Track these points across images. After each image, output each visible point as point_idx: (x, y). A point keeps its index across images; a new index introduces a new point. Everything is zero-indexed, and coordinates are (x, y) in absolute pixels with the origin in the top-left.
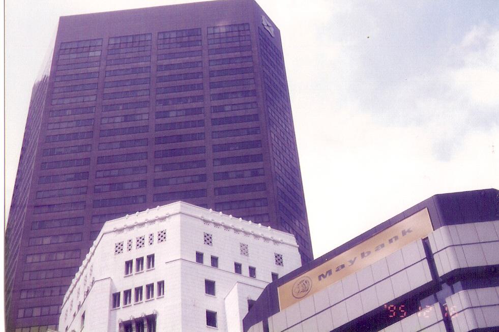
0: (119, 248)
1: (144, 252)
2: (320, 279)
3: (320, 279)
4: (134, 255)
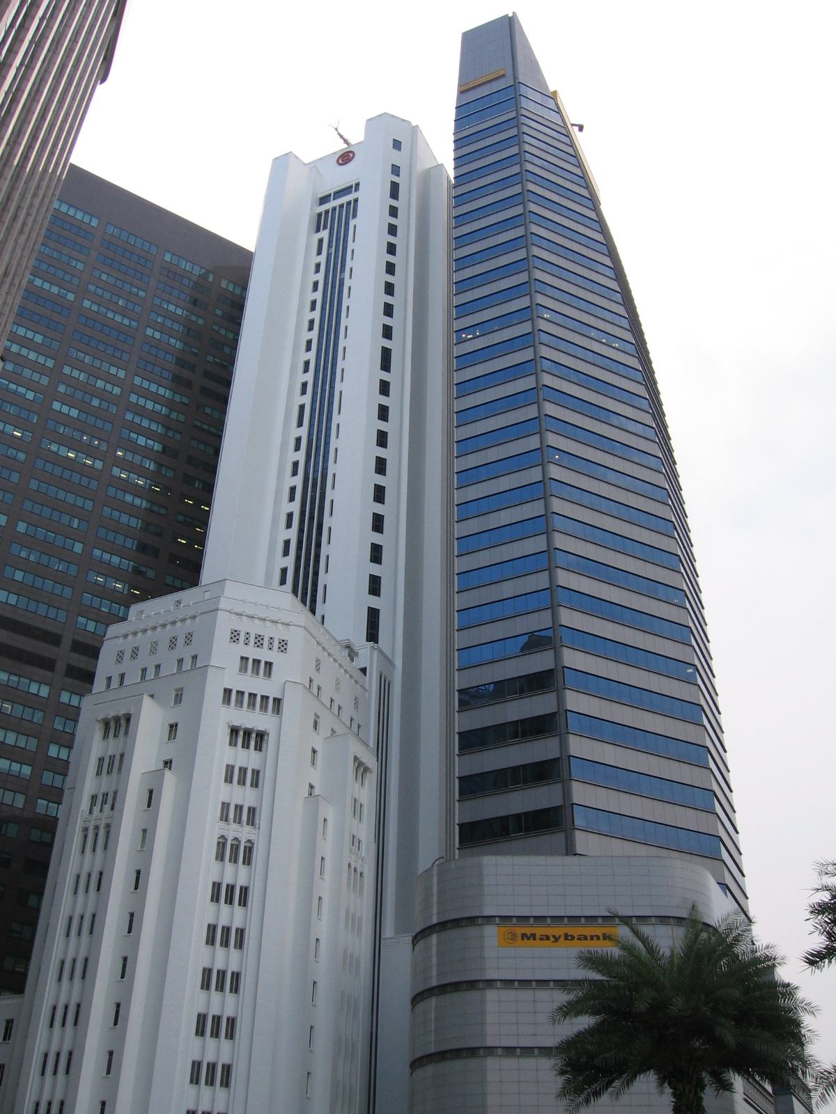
0: (235, 637)
1: (264, 655)
2: (523, 939)
3: (523, 939)
4: (252, 653)
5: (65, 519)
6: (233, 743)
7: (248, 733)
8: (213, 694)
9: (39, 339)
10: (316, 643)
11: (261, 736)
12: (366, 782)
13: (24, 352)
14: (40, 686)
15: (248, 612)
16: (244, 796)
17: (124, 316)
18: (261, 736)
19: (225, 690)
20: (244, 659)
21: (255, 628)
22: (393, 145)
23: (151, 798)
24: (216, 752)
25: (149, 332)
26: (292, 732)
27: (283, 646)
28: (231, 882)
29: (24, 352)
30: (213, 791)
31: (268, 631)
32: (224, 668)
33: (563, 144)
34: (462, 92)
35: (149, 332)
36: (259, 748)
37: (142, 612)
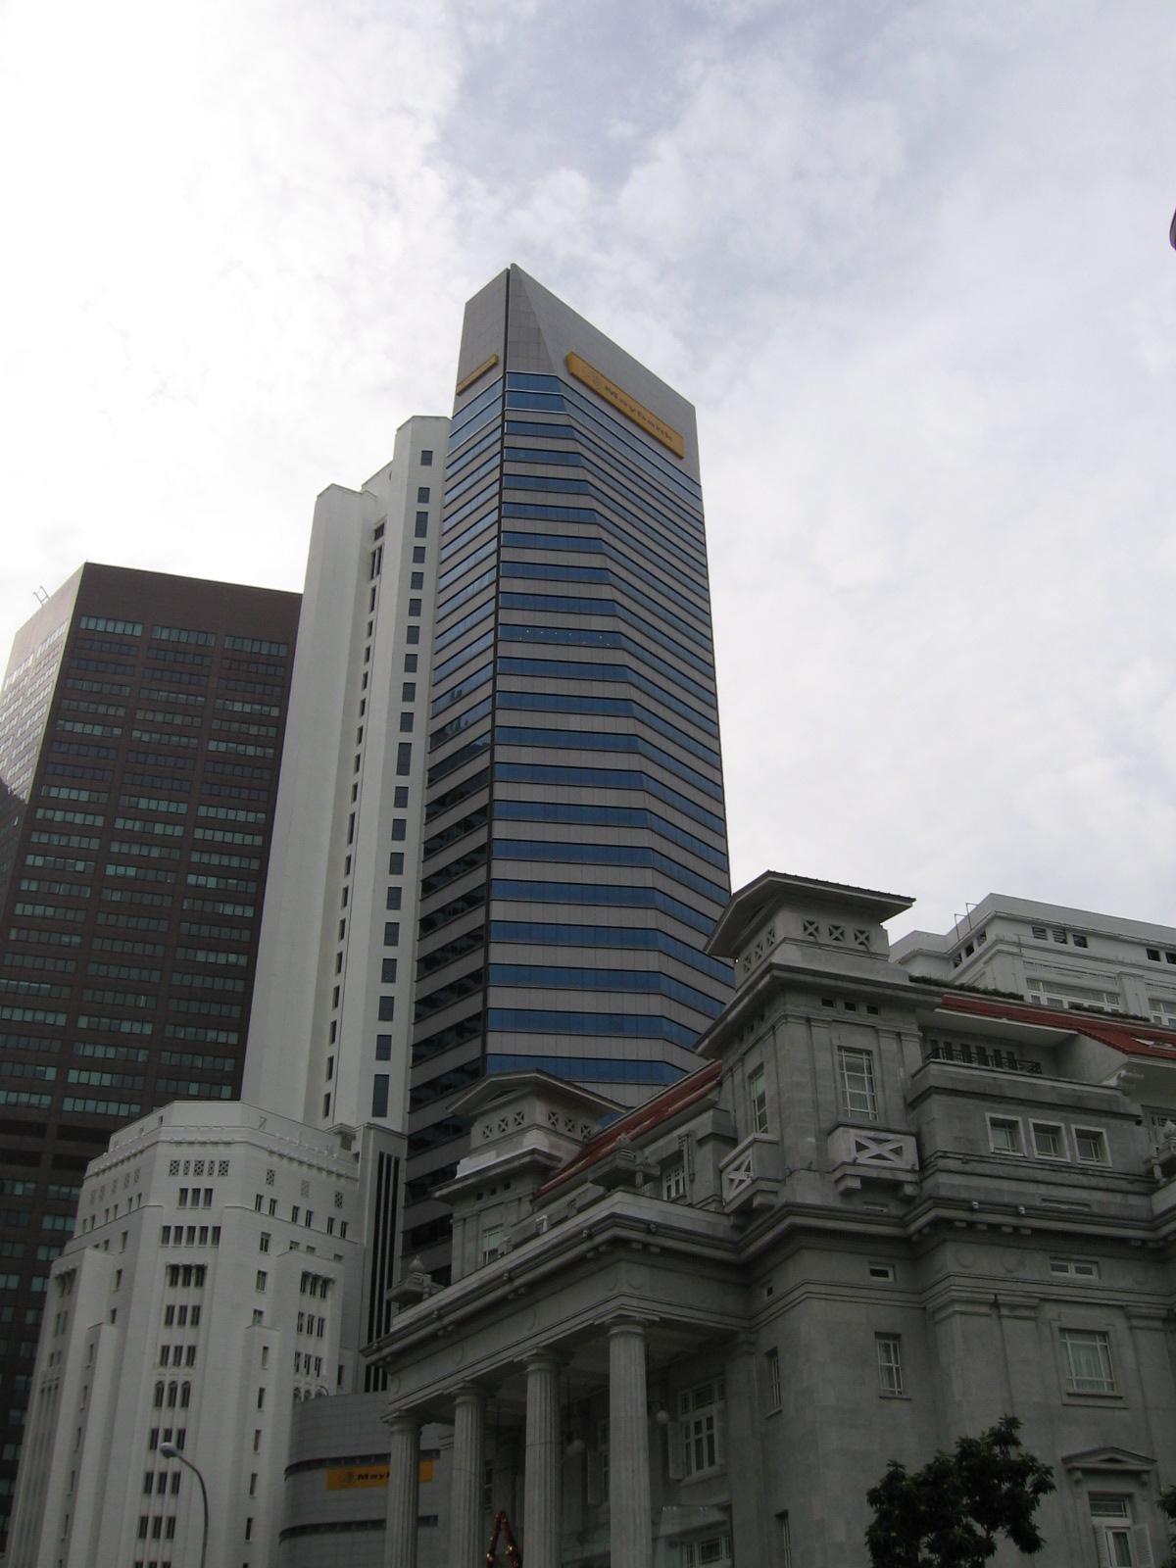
1: (203, 1182)
4: (191, 1182)
5: (130, 999)
6: (173, 1283)
7: (188, 1269)
8: (151, 1233)
9: (84, 796)
10: (267, 1154)
11: (201, 1270)
12: (329, 1294)
13: (69, 817)
14: (54, 1221)
15: (176, 1139)
16: (180, 1336)
17: (181, 736)
18: (201, 1270)
19: (165, 1228)
20: (184, 1191)
21: (193, 1154)
22: (419, 496)
23: (92, 1349)
24: (154, 1292)
25: (212, 746)
26: (230, 1265)
27: (224, 1168)
28: (168, 1427)
29: (69, 817)
30: (150, 1333)
31: (209, 1154)
32: (163, 1206)
33: (466, 570)
34: (459, 394)
35: (212, 746)
36: (200, 1282)
37: (142, 1130)
